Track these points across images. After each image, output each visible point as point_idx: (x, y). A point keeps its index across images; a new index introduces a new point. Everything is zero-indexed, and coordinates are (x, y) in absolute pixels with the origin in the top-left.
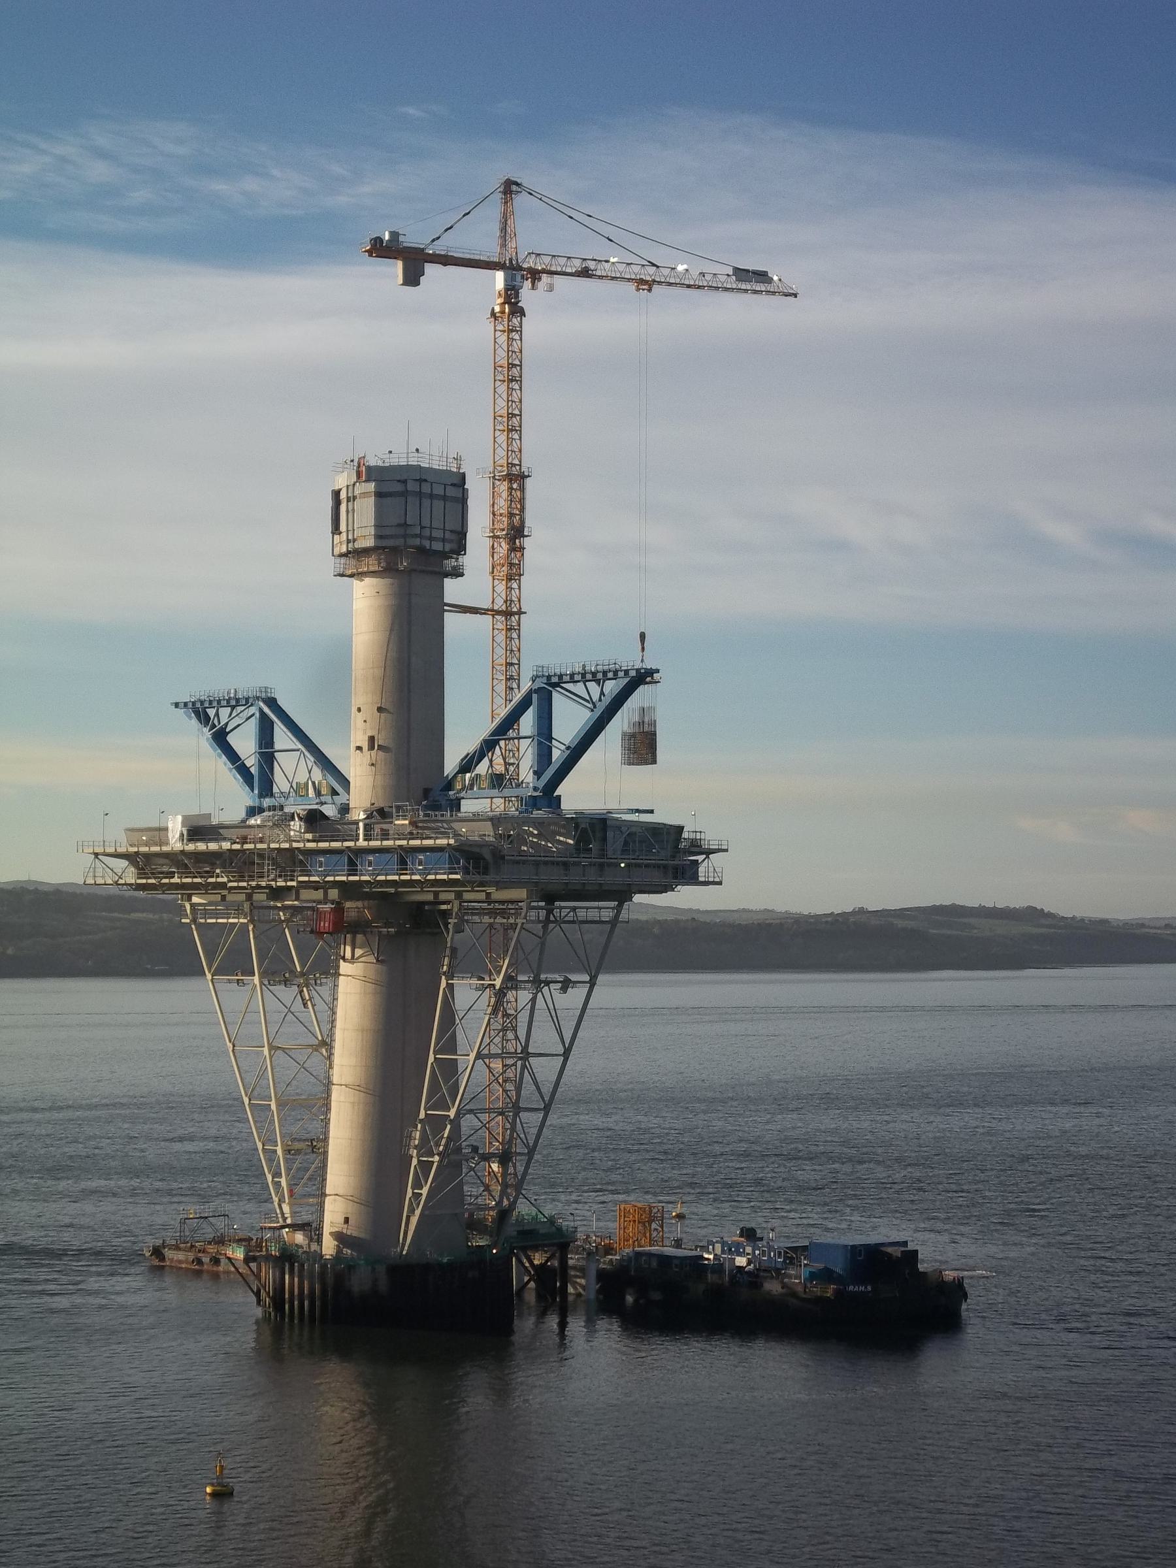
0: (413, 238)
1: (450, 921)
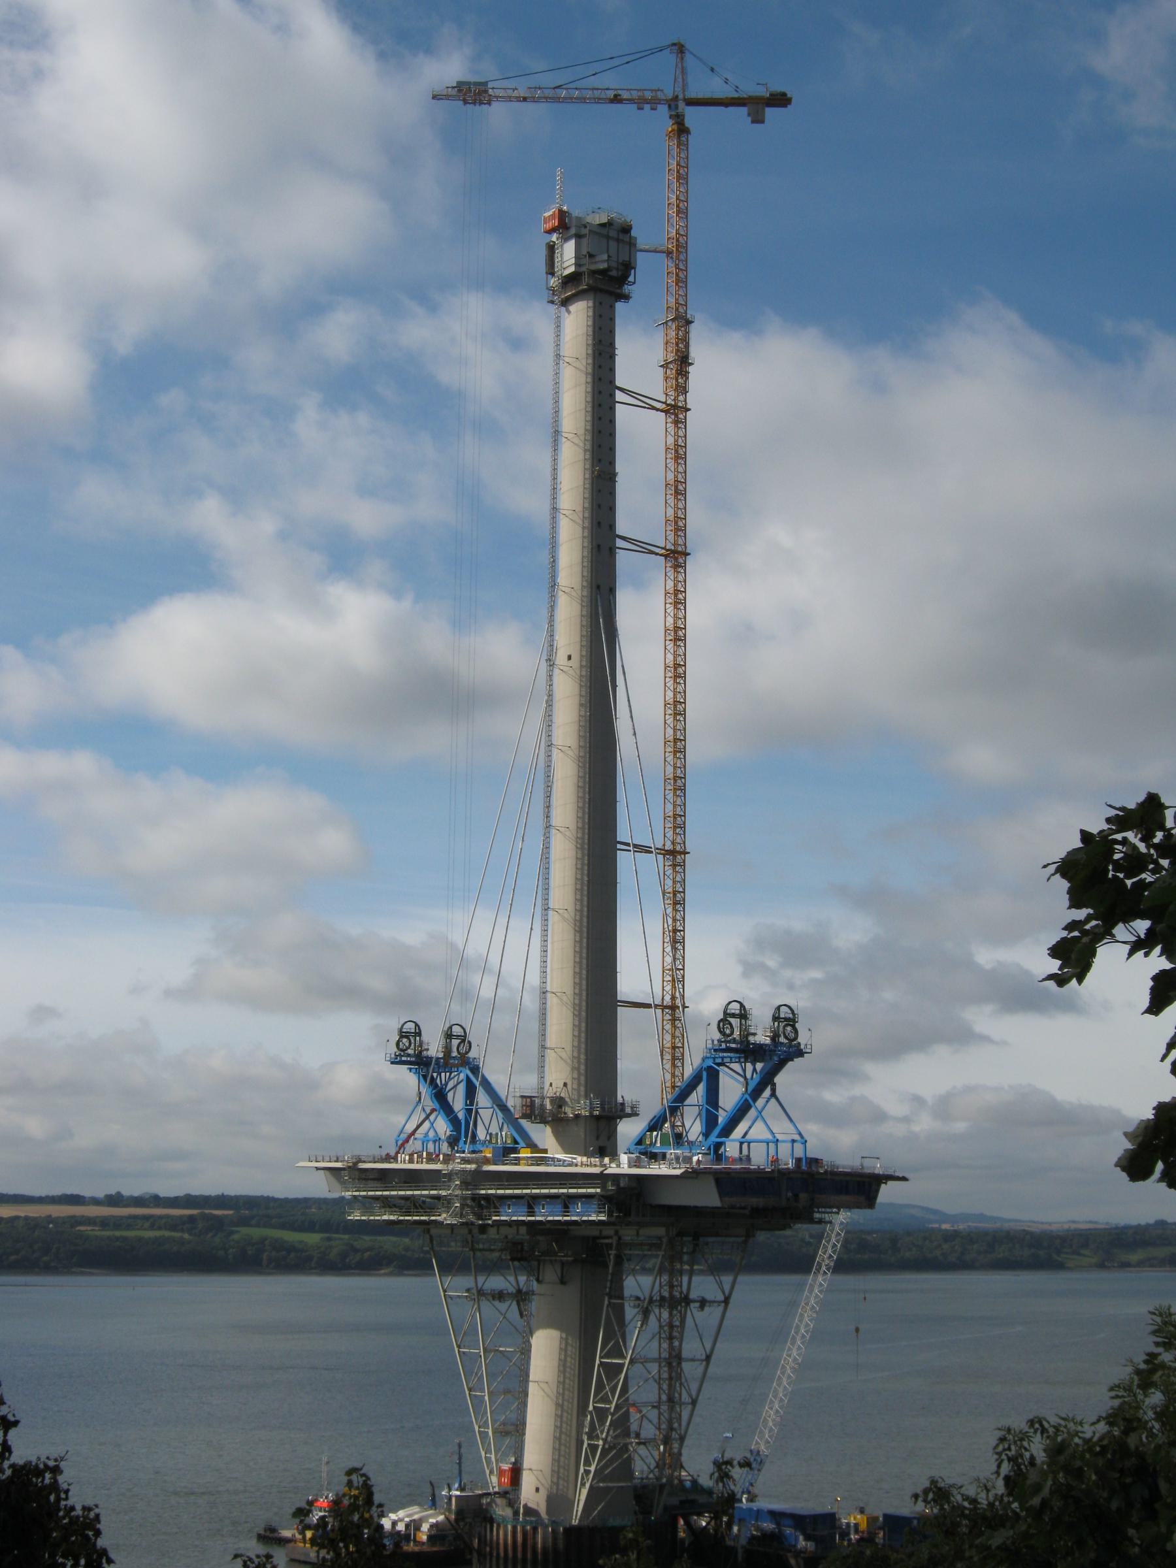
1: (610, 1252)
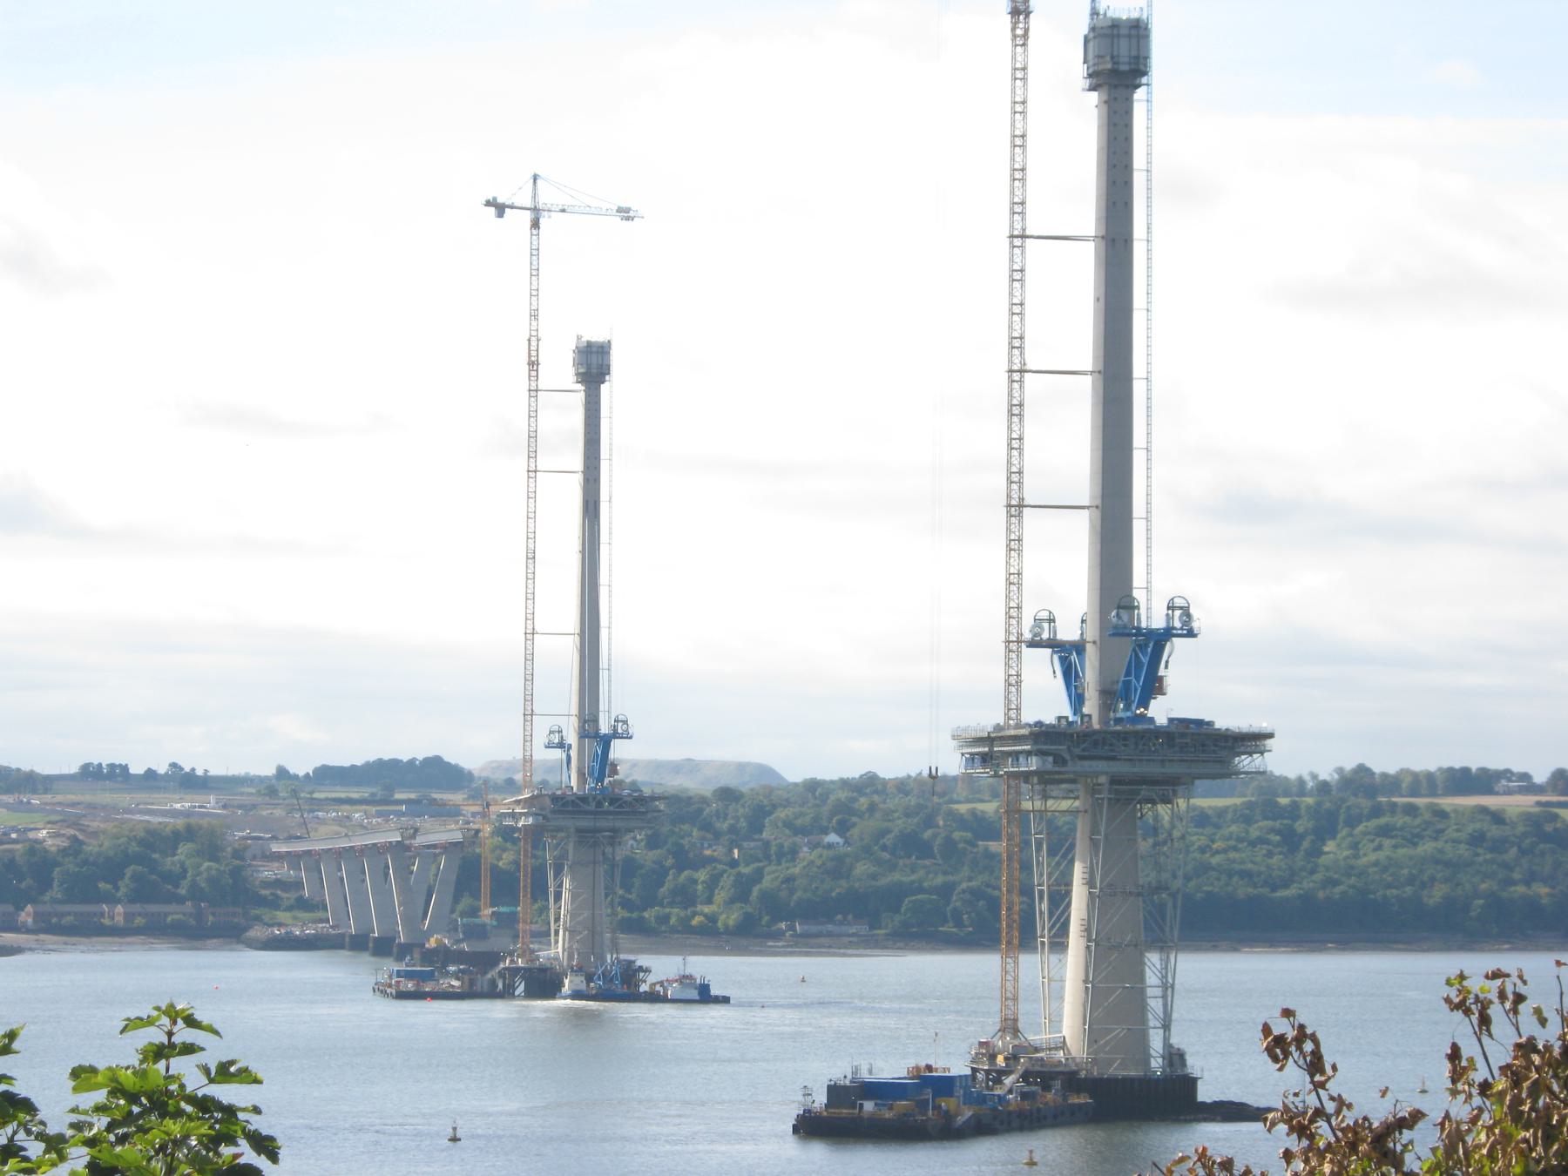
0: (500, 200)
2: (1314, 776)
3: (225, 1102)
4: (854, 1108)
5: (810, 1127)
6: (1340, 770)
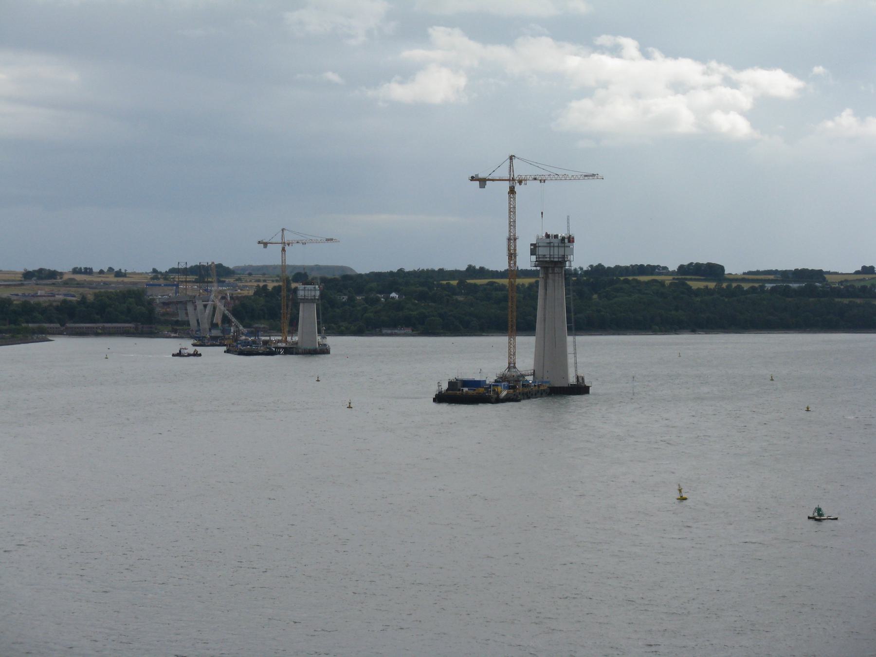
0: (481, 176)
2: (581, 269)
3: (746, 272)
4: (460, 391)
5: (440, 398)
6: (591, 266)
